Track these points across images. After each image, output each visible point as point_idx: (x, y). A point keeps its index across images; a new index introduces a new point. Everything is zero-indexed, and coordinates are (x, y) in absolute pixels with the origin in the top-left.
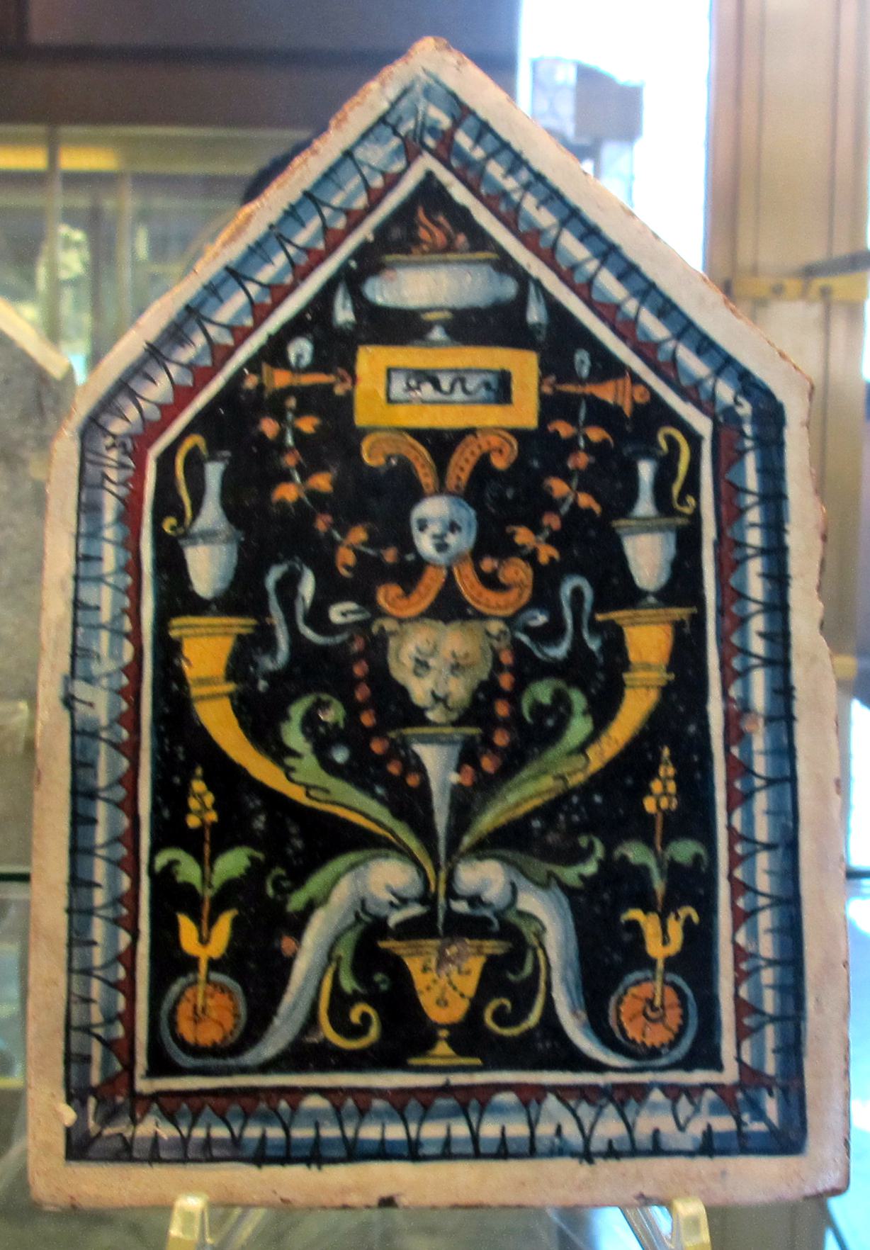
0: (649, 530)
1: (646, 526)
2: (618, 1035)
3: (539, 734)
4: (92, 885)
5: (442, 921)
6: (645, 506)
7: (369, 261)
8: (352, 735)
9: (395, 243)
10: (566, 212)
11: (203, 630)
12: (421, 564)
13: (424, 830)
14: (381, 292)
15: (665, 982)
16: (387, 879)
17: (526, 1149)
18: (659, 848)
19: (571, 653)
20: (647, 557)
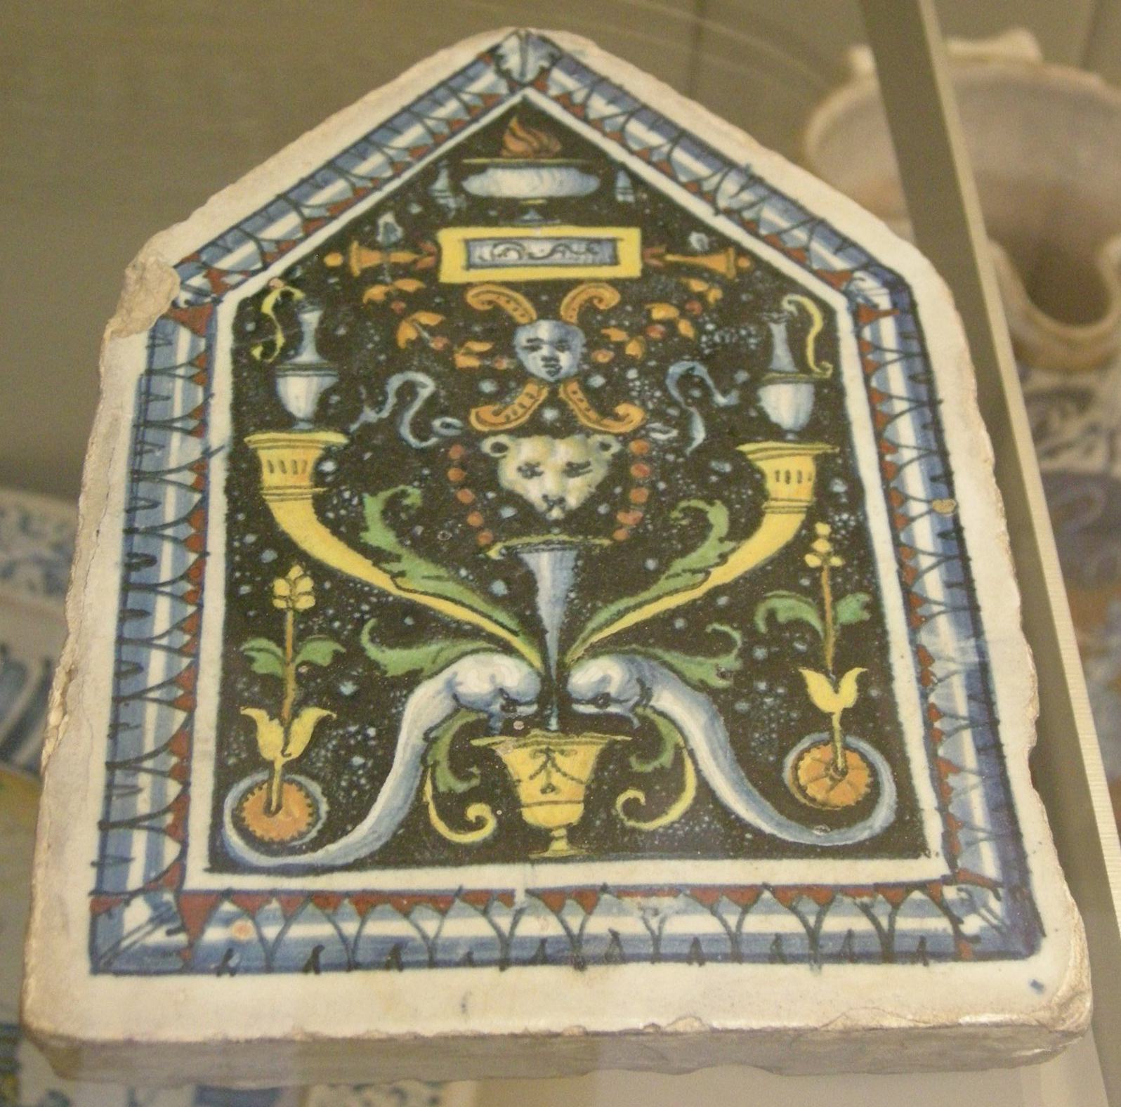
0: (786, 381)
1: (785, 378)
2: (798, 796)
3: (670, 540)
4: (363, 916)
5: (554, 705)
6: (782, 356)
7: (460, 164)
8: (427, 514)
9: (489, 146)
10: (745, 949)
11: (274, 491)
12: (522, 376)
13: (532, 628)
14: (476, 185)
15: (846, 747)
16: (486, 675)
17: (471, 243)
18: (828, 598)
19: (710, 429)
20: (785, 402)
